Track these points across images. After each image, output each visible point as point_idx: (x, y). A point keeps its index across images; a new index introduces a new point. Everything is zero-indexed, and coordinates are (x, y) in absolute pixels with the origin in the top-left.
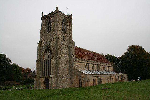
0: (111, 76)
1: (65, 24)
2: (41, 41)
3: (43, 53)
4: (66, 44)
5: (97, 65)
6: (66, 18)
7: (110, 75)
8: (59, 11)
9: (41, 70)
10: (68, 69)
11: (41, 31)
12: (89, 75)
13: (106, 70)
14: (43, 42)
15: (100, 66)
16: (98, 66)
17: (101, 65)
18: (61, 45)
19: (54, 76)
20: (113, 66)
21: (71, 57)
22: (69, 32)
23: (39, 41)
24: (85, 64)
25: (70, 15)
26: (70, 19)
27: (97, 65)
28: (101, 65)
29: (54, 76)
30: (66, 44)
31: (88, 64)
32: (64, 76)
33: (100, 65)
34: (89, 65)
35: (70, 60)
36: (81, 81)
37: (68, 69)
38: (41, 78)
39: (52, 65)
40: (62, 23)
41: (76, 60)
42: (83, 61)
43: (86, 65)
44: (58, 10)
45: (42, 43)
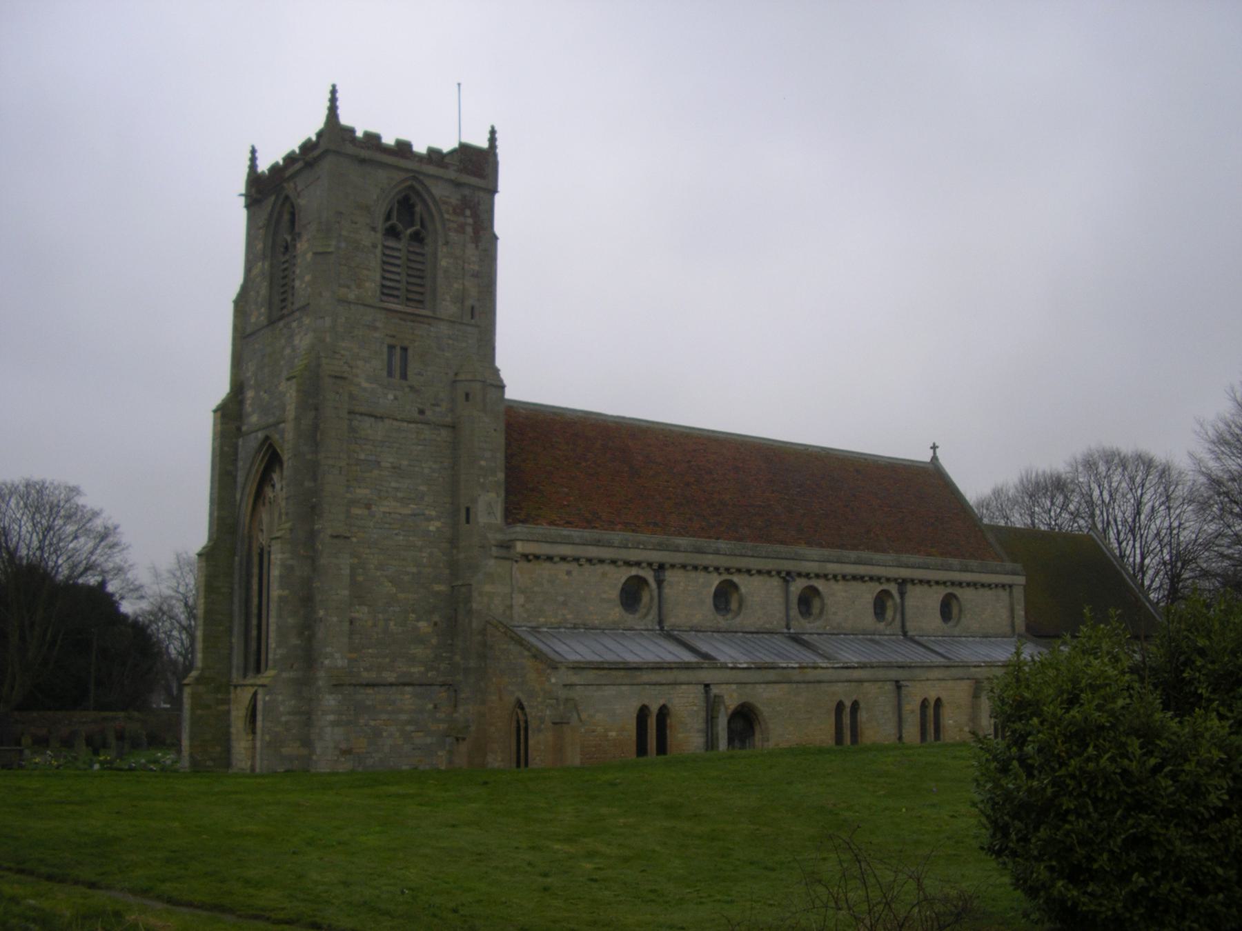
0: (898, 686)
1: (417, 238)
2: (238, 387)
3: (252, 488)
4: (422, 412)
5: (776, 582)
6: (428, 182)
7: (894, 674)
8: (351, 131)
9: (237, 628)
10: (436, 618)
11: (241, 304)
12: (591, 675)
13: (908, 624)
14: (250, 394)
15: (819, 584)
16: (797, 586)
17: (974, 585)
18: (368, 421)
19: (292, 674)
20: (1021, 580)
21: (468, 521)
22: (460, 299)
23: (221, 388)
24: (715, 580)
25: (483, 143)
26: (473, 180)
27: (787, 577)
28: (974, 585)
29: (292, 674)
30: (422, 412)
31: (903, 583)
32: (391, 677)
33: (960, 584)
34: (669, 575)
35: (454, 542)
36: (526, 722)
37: (436, 618)
38: (236, 687)
39: (275, 592)
40: (392, 232)
41: (506, 546)
42: (593, 552)
43: (885, 594)
44: (345, 119)
45: (241, 403)
